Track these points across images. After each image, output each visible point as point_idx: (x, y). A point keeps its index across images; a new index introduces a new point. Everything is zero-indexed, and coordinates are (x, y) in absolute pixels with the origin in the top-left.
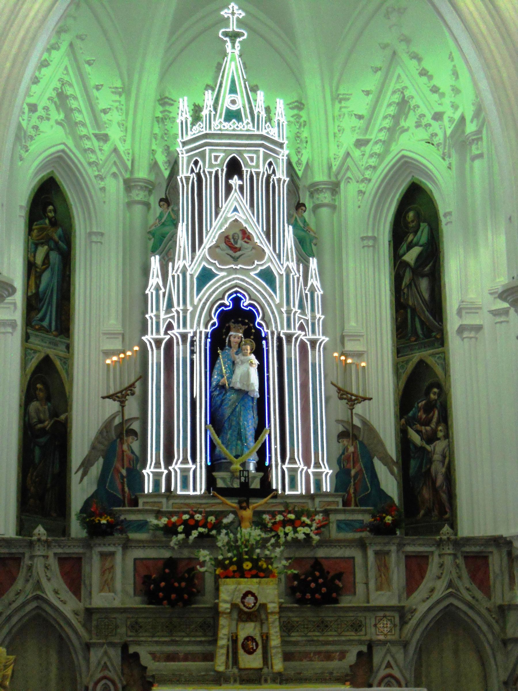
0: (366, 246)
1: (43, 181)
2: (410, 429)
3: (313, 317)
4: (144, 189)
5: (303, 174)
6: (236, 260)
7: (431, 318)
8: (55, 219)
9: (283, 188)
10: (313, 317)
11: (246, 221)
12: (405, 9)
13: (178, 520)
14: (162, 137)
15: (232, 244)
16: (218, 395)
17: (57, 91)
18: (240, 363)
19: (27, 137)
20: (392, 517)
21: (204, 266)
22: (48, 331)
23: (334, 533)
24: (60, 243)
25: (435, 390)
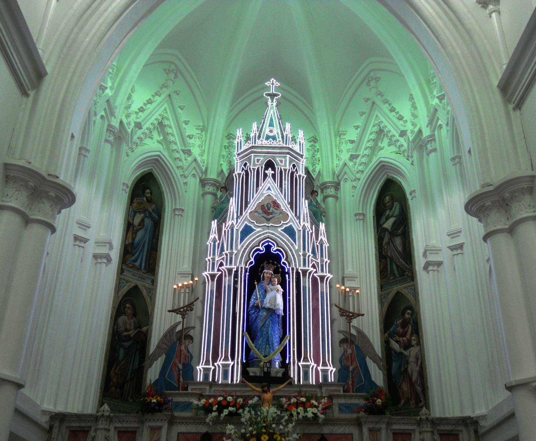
0: (359, 219)
1: (144, 174)
2: (391, 340)
3: (322, 261)
4: (213, 185)
5: (316, 177)
6: (268, 220)
7: (404, 262)
8: (151, 199)
9: (303, 181)
10: (322, 261)
11: (276, 196)
12: (380, 78)
13: (214, 401)
14: (227, 156)
15: (266, 210)
16: (254, 312)
17: (158, 121)
18: (270, 291)
19: (133, 143)
20: (382, 400)
21: (246, 224)
22: (139, 269)
23: (336, 413)
24: (153, 214)
25: (409, 311)
